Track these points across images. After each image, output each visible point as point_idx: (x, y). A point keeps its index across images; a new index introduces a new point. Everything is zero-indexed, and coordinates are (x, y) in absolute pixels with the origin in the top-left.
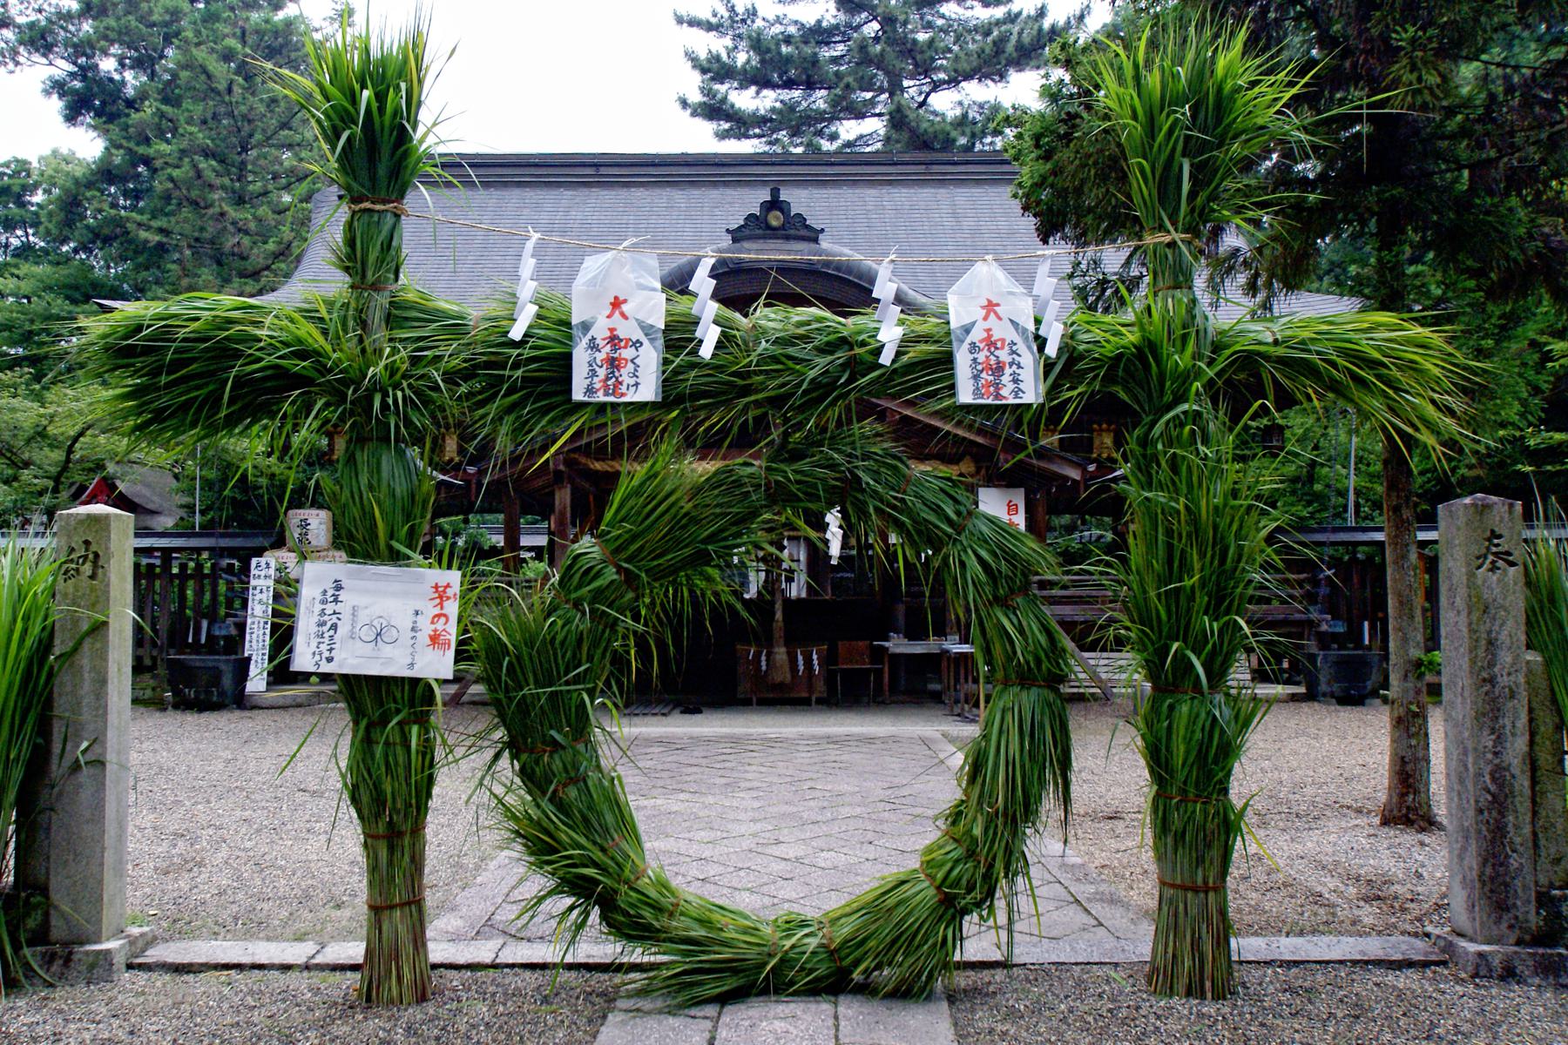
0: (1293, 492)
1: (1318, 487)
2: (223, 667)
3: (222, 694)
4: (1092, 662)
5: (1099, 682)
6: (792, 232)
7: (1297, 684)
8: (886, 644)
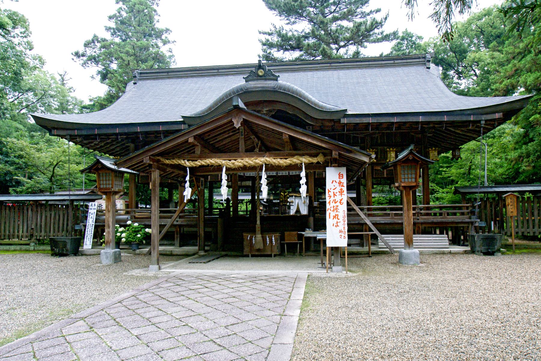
0: (463, 178)
1: (472, 176)
2: (67, 241)
3: (67, 250)
4: (385, 239)
5: (388, 247)
6: (267, 77)
7: (467, 246)
8: (303, 233)
